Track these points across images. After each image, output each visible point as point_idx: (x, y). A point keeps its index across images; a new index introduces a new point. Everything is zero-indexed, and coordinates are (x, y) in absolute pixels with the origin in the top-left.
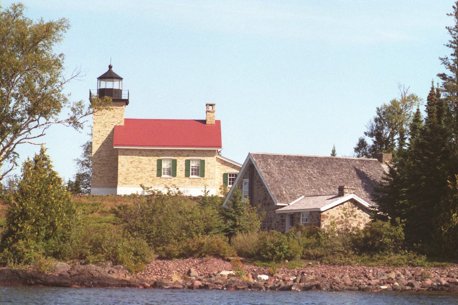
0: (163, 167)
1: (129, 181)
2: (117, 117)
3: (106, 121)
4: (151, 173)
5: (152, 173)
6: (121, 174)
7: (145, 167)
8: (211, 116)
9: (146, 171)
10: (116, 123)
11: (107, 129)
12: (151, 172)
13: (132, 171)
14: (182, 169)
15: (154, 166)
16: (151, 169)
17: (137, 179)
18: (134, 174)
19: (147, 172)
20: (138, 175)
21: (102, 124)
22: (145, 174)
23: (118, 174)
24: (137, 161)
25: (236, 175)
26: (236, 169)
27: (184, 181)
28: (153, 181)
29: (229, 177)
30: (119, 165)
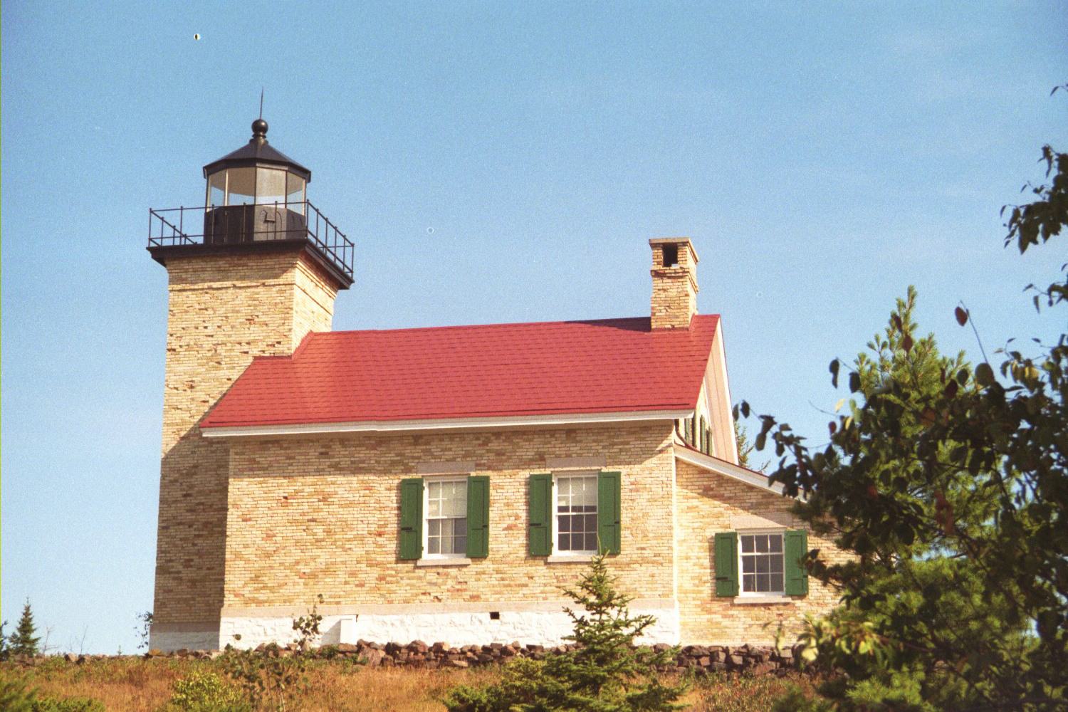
0: (426, 515)
1: (272, 589)
2: (263, 318)
3: (220, 338)
4: (371, 547)
5: (375, 543)
6: (238, 556)
7: (350, 518)
8: (673, 292)
9: (350, 535)
10: (262, 346)
11: (223, 373)
12: (371, 540)
13: (285, 538)
14: (511, 521)
15: (387, 514)
16: (373, 528)
17: (313, 576)
18: (297, 554)
19: (355, 539)
20: (314, 559)
21: (203, 353)
22: (345, 550)
23: (228, 556)
24: (310, 495)
25: (776, 540)
26: (755, 508)
27: (525, 580)
28: (383, 585)
29: (740, 553)
30: (233, 516)
